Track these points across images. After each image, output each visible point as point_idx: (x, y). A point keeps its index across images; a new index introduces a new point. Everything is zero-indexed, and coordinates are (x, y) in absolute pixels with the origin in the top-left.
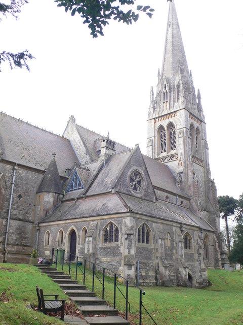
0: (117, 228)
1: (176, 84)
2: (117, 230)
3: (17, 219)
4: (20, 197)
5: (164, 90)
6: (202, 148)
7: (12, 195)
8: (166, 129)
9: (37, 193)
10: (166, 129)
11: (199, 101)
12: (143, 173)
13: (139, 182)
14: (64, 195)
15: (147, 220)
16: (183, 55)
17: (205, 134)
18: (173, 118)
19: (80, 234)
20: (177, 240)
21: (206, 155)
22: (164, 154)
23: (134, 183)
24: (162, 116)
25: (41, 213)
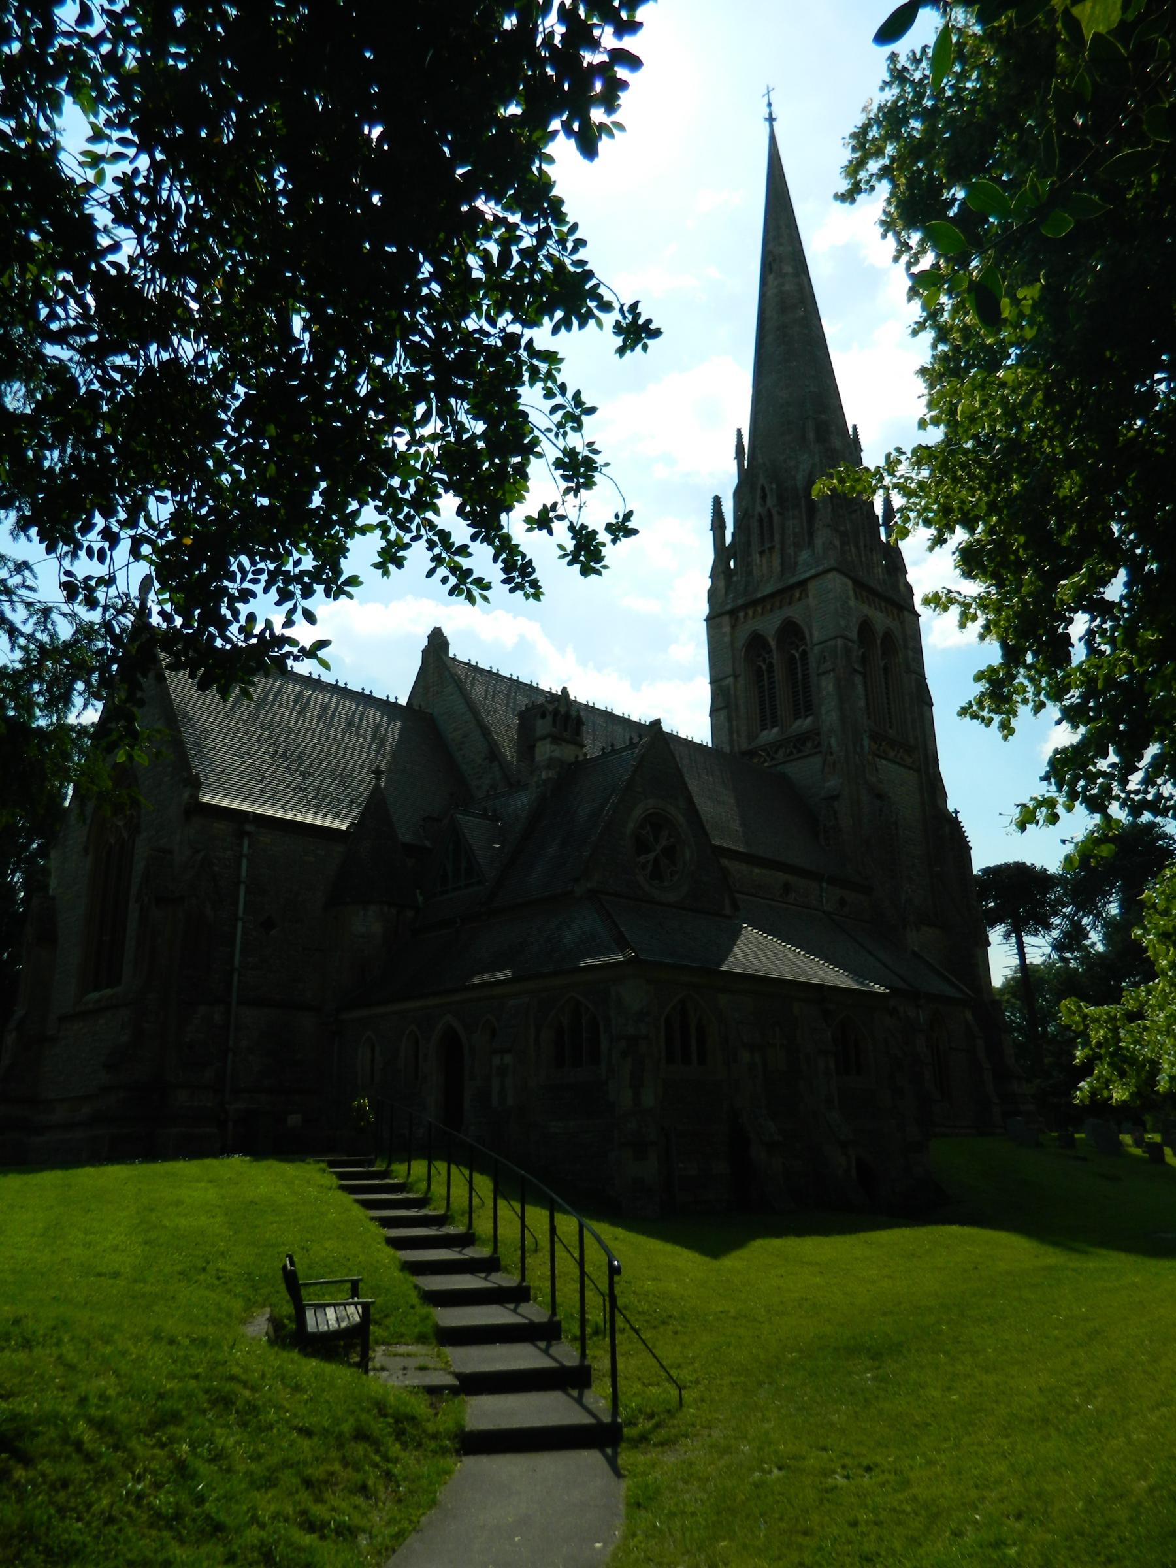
5: (759, 509)
8: (773, 643)
10: (773, 643)
22: (771, 734)
23: (652, 856)
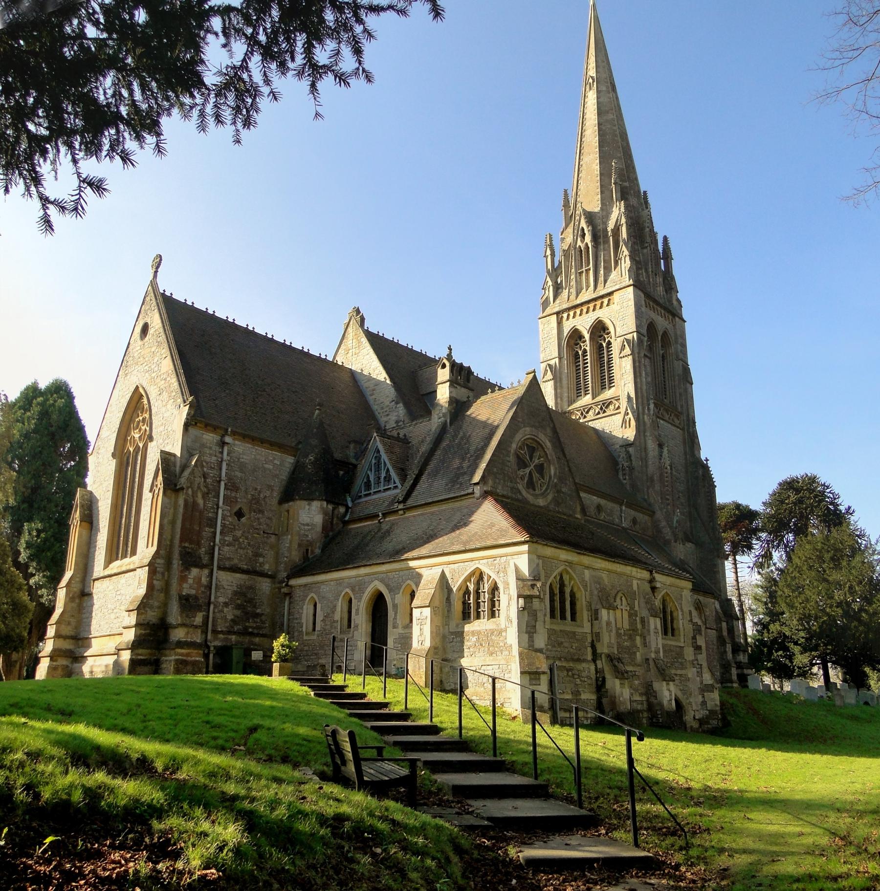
1: (611, 225)
3: (234, 569)
4: (239, 514)
5: (579, 243)
6: (677, 382)
7: (220, 511)
8: (587, 336)
12: (549, 444)
14: (347, 508)
15: (570, 564)
18: (605, 309)
23: (527, 471)
25: (294, 553)
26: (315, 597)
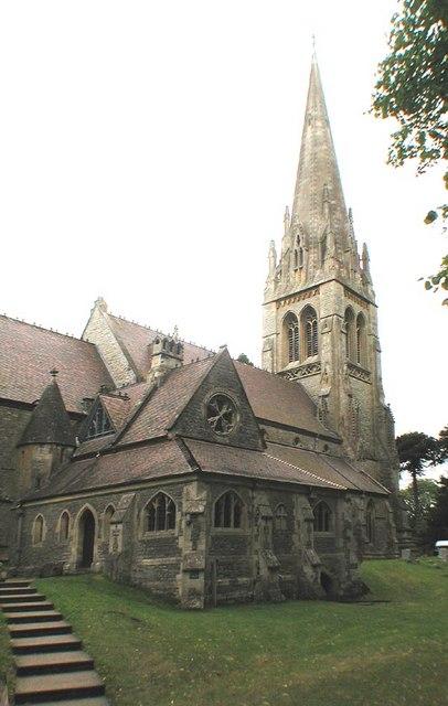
0: (172, 503)
2: (172, 508)
5: (296, 247)
8: (299, 318)
9: (18, 447)
10: (299, 318)
11: (366, 265)
13: (228, 416)
14: (75, 448)
16: (336, 179)
17: (375, 324)
19: (100, 516)
20: (300, 518)
21: (376, 361)
22: (294, 365)
23: (217, 418)
24: (290, 296)
26: (91, 508)
